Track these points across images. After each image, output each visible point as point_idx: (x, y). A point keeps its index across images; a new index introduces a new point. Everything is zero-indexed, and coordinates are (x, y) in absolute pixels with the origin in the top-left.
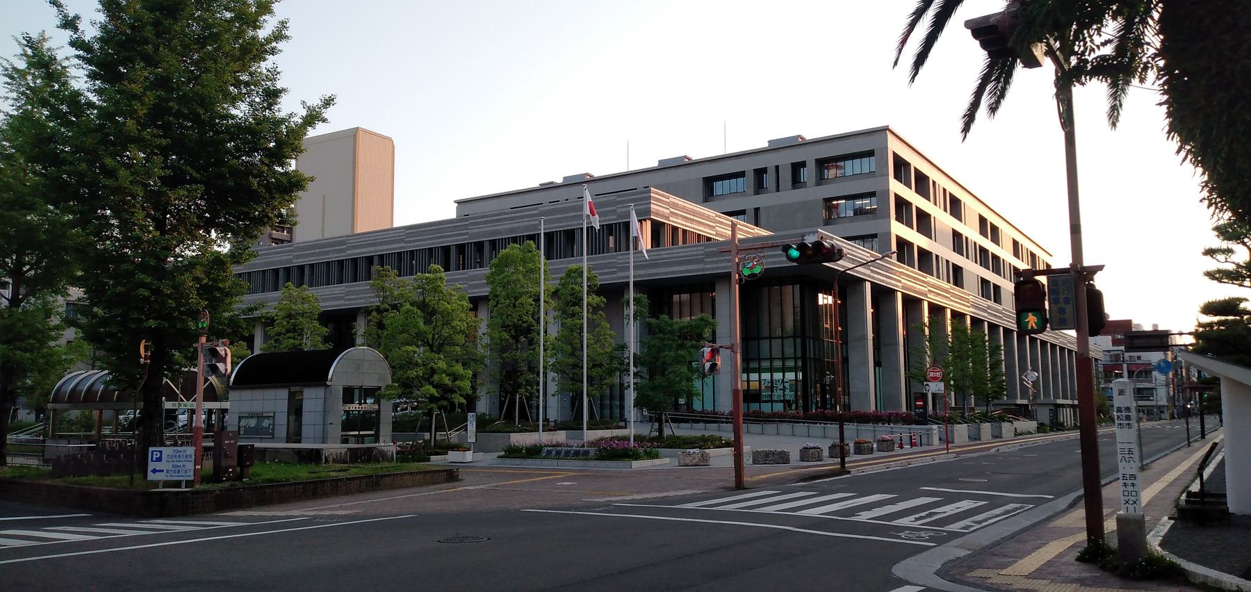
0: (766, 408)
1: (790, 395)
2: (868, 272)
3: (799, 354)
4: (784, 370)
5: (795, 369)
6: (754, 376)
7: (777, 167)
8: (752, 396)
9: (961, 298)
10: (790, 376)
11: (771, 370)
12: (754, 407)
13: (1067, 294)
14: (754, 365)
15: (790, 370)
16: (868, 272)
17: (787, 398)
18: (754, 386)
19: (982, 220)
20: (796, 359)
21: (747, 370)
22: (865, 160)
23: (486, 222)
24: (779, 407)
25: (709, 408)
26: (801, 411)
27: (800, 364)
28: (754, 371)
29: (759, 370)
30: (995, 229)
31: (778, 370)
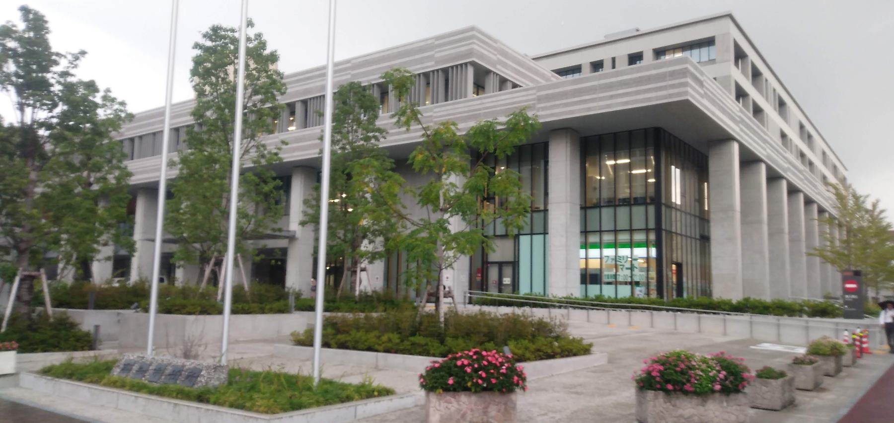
0: (608, 291)
1: (639, 276)
2: (737, 129)
3: (652, 225)
4: (631, 245)
5: (647, 244)
6: (594, 253)
7: (614, 60)
8: (589, 278)
9: (811, 183)
10: (640, 252)
11: (615, 245)
12: (594, 290)
13: (506, 345)
14: (593, 238)
15: (639, 245)
16: (737, 129)
17: (636, 279)
18: (594, 264)
19: (802, 127)
20: (647, 230)
21: (585, 245)
22: (704, 50)
23: (298, 81)
24: (624, 292)
25: (538, 289)
26: (654, 295)
27: (652, 237)
28: (593, 246)
29: (600, 245)
30: (810, 137)
31: (624, 245)
